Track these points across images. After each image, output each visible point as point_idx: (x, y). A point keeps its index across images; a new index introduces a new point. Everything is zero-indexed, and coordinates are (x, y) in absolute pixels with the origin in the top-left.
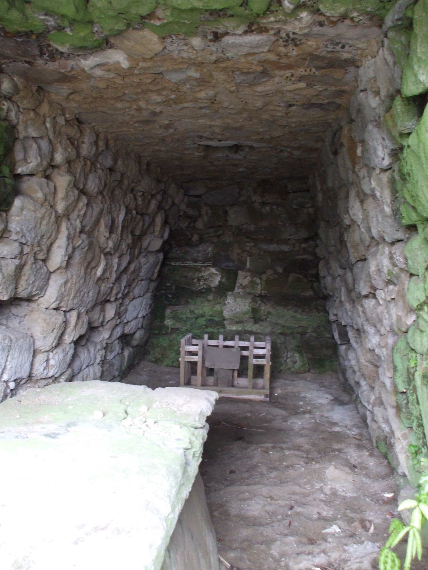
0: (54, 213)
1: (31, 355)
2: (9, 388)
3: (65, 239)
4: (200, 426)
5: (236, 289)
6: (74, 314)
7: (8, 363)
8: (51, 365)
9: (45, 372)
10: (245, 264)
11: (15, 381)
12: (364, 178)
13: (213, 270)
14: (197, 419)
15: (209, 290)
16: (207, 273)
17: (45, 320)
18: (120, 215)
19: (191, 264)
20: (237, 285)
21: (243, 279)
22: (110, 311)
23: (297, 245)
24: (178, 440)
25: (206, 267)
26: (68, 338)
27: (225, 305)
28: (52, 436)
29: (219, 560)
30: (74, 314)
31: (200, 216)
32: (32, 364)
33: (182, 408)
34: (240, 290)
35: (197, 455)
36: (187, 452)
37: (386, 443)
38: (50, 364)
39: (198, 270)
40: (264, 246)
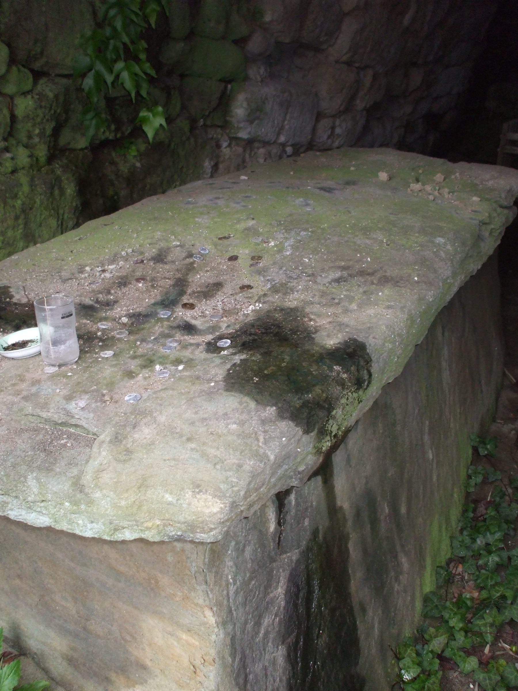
1: (314, 119)
2: (286, 153)
4: (505, 204)
6: (370, 73)
7: (286, 122)
8: (337, 134)
9: (330, 141)
11: (293, 145)
14: (503, 196)
22: (416, 78)
24: (475, 211)
26: (360, 104)
28: (329, 190)
29: (504, 374)
30: (370, 73)
32: (314, 130)
33: (487, 183)
35: (496, 234)
36: (483, 228)
38: (336, 133)
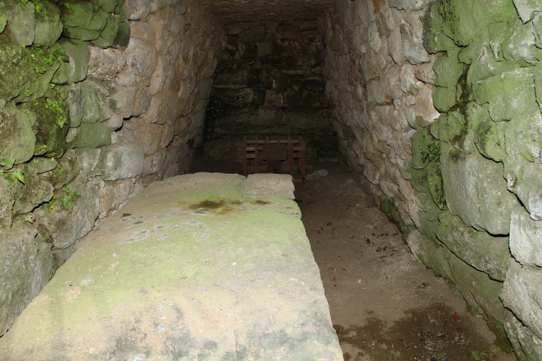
0: (154, 50)
3: (161, 70)
5: (265, 103)
10: (271, 84)
12: (388, 17)
13: (249, 90)
15: (245, 105)
16: (244, 92)
17: (150, 132)
18: (190, 51)
19: (233, 86)
20: (266, 100)
21: (270, 95)
23: (308, 70)
25: (243, 88)
27: (257, 115)
31: (237, 50)
34: (268, 104)
37: (164, 242)
39: (238, 90)
40: (285, 71)
